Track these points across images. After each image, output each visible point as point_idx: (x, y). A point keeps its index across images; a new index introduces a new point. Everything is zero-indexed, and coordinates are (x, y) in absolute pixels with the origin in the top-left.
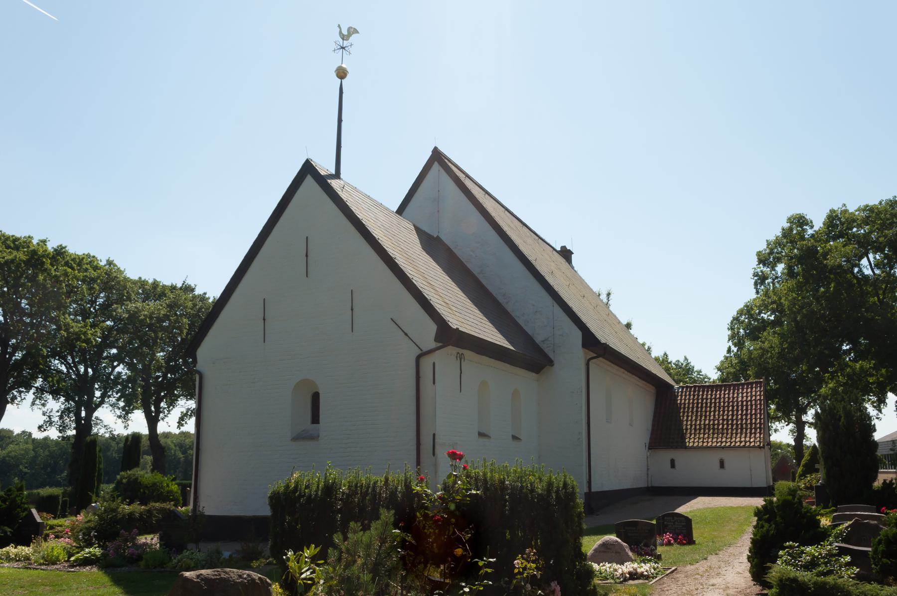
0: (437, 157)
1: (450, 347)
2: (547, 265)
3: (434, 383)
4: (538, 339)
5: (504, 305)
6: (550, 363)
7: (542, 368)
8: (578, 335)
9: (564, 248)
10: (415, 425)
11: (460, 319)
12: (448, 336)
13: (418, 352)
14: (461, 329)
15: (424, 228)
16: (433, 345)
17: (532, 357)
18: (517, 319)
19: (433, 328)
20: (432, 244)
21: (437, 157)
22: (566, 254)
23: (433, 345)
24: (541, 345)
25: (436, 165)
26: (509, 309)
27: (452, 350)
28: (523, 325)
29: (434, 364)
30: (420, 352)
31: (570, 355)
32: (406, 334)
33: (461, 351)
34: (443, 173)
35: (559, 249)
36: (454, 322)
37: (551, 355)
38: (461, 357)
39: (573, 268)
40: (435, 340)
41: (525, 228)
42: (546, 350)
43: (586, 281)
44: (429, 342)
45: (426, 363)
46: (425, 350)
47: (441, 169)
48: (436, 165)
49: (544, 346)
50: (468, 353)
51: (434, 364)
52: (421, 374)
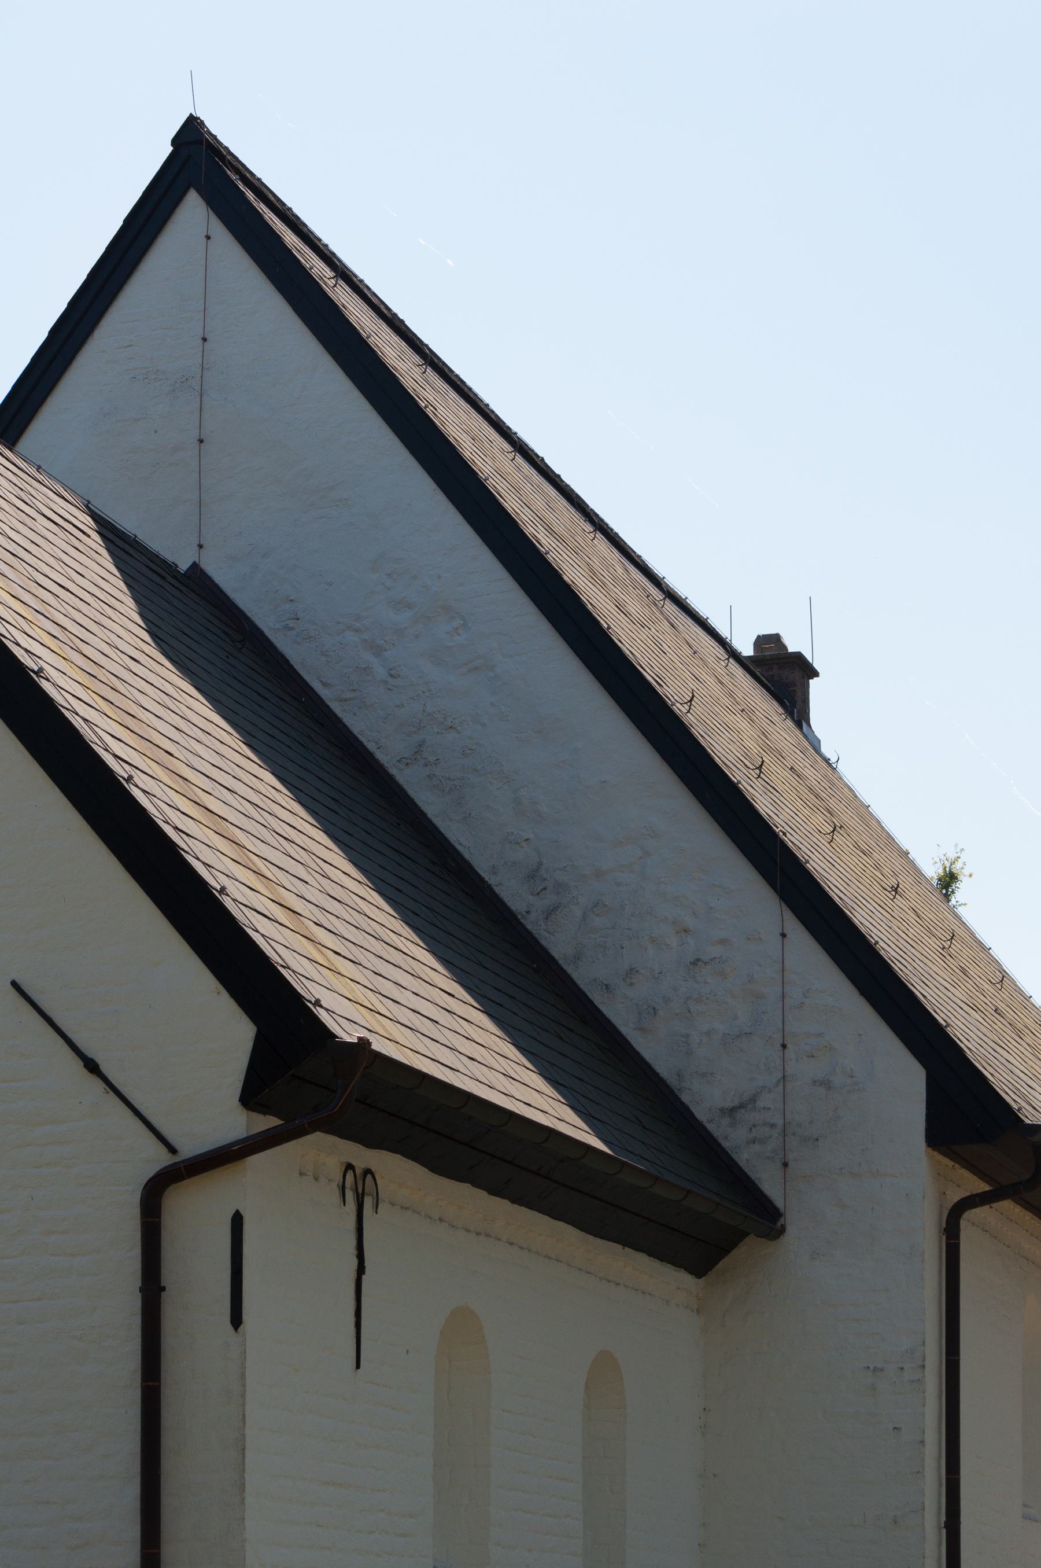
0: (197, 165)
1: (318, 1137)
2: (731, 725)
3: (236, 1319)
4: (705, 1100)
5: (533, 923)
6: (766, 1218)
7: (723, 1250)
8: (906, 1080)
9: (769, 643)
10: (134, 1532)
11: (359, 993)
12: (304, 1072)
13: (158, 1159)
14: (378, 1045)
15: (128, 523)
16: (235, 1124)
17: (668, 1188)
18: (597, 998)
19: (231, 1035)
20: (193, 615)
21: (197, 165)
22: (782, 674)
23: (235, 1124)
24: (719, 1129)
25: (193, 213)
26: (559, 945)
27: (324, 1152)
28: (626, 1027)
29: (237, 1221)
30: (162, 1159)
31: (868, 1178)
32: (92, 1067)
33: (364, 1157)
34: (228, 250)
35: (747, 650)
36: (344, 1016)
37: (770, 1185)
38: (360, 1189)
39: (815, 744)
40: (251, 1096)
41: (602, 544)
42: (744, 1158)
43: (880, 810)
44: (211, 1108)
45: (197, 1217)
46: (190, 1148)
47: (218, 229)
48: (193, 213)
49: (732, 1138)
50: (393, 1170)
51: (237, 1221)
52: (170, 1274)
